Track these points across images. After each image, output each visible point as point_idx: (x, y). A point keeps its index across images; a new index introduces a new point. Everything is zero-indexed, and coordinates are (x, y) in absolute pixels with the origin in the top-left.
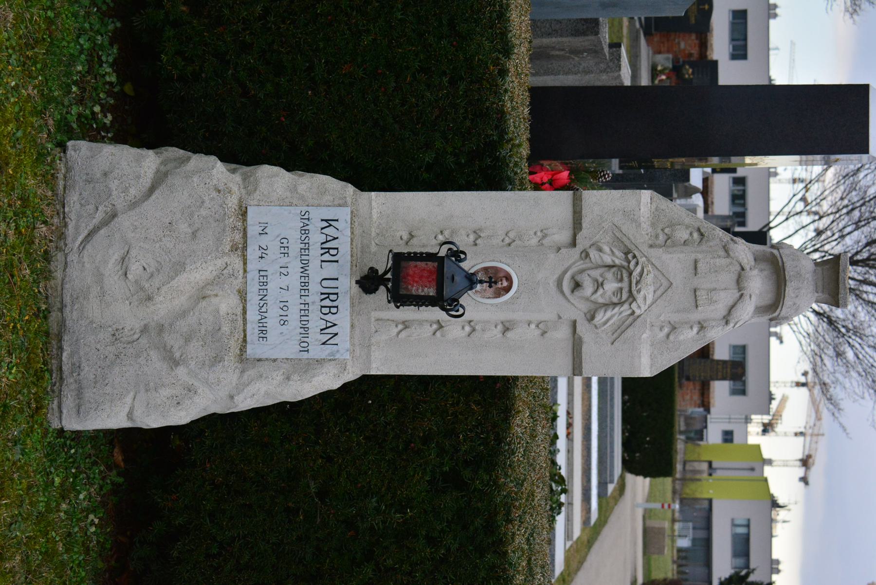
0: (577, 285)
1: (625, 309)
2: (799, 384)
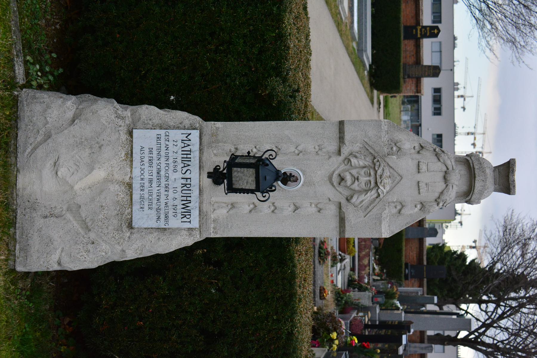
1: (372, 194)
2: (471, 247)
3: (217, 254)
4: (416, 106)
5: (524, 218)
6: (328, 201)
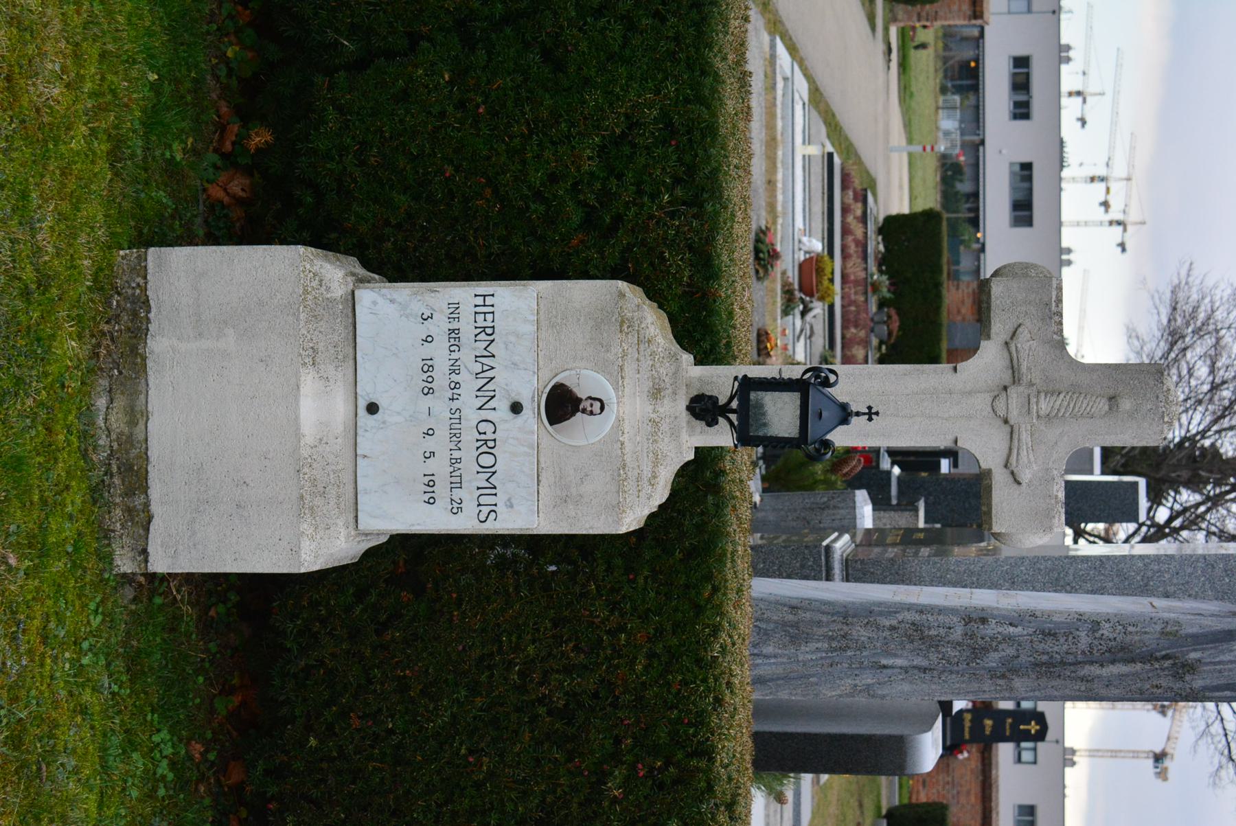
4: (972, 98)
5: (1215, 287)
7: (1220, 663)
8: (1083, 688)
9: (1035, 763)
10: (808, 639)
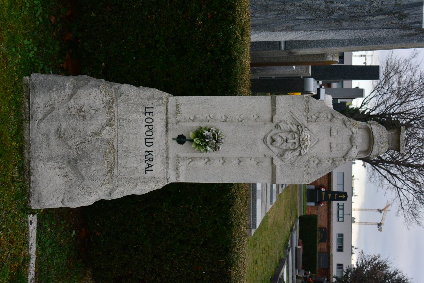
0: (273, 141)
3: (175, 193)
6: (263, 156)
7: (415, 14)
8: (367, 25)
9: (343, 221)
10: (271, 10)
